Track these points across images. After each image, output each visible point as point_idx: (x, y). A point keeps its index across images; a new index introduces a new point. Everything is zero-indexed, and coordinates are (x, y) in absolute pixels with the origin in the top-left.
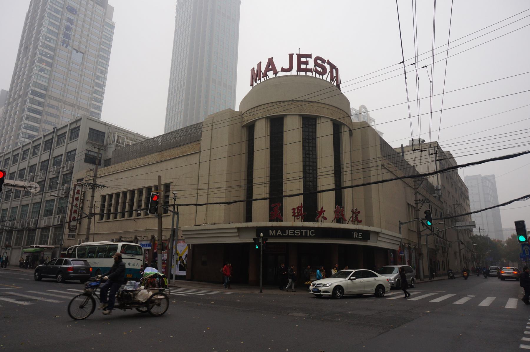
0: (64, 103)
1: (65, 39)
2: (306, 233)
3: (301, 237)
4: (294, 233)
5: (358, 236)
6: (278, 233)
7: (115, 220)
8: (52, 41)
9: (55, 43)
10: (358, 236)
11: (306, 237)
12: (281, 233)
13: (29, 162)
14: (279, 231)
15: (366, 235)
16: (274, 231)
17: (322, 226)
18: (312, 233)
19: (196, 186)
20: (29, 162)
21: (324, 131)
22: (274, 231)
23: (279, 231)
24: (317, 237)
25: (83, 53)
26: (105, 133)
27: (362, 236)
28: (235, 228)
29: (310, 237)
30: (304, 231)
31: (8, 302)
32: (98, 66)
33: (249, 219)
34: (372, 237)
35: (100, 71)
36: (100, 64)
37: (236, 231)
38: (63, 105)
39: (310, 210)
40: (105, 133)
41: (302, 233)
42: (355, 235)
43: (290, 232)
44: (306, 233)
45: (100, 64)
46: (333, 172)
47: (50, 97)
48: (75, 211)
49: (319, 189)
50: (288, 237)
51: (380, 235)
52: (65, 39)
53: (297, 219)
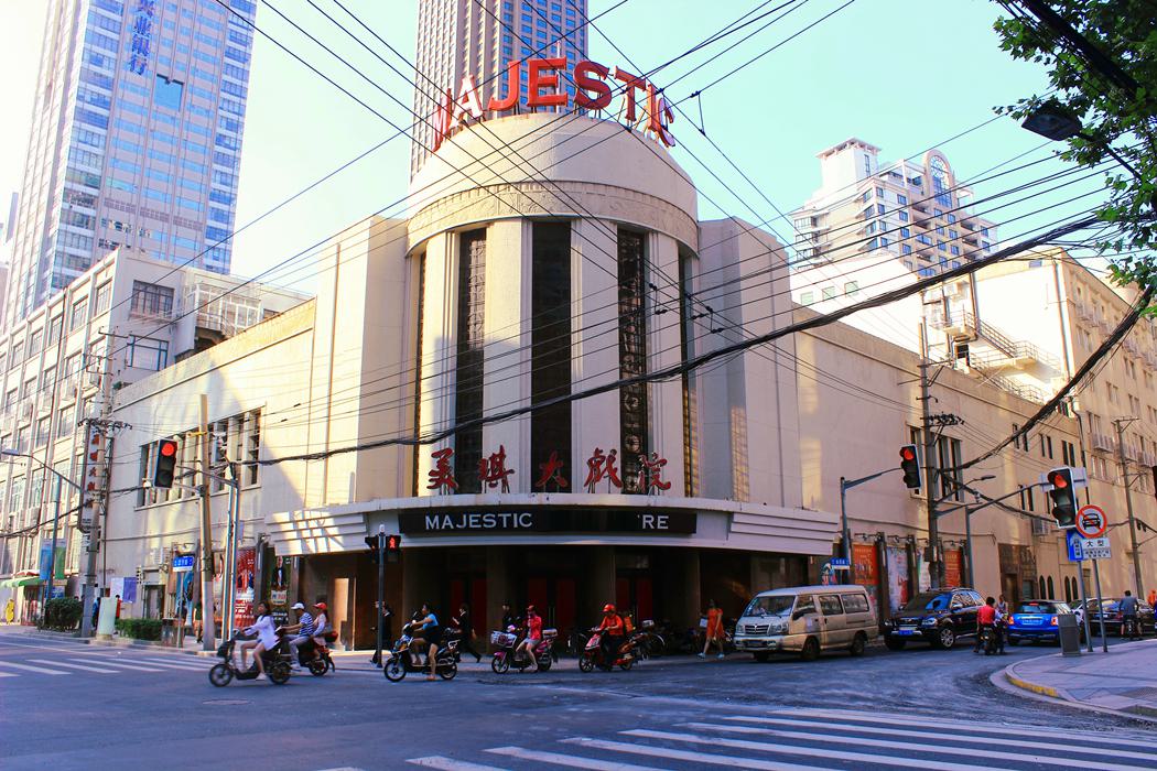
0: (142, 214)
1: (135, 52)
2: (510, 520)
3: (499, 530)
4: (481, 521)
5: (655, 523)
6: (445, 524)
7: (221, 492)
8: (106, 63)
9: (112, 66)
10: (655, 523)
11: (511, 530)
12: (450, 524)
13: (23, 374)
14: (447, 517)
15: (683, 521)
16: (437, 518)
17: (551, 502)
18: (526, 520)
19: (312, 417)
20: (23, 374)
21: (663, 256)
22: (437, 518)
23: (447, 517)
24: (537, 529)
25: (182, 84)
26: (172, 290)
27: (668, 522)
28: (359, 514)
29: (521, 531)
30: (505, 516)
31: (705, 764)
32: (221, 112)
33: (167, 499)
34: (701, 522)
35: (224, 123)
36: (225, 106)
37: (360, 519)
38: (141, 218)
39: (636, 457)
40: (172, 290)
41: (499, 520)
42: (647, 520)
43: (472, 520)
44: (510, 520)
45: (225, 106)
46: (485, 380)
47: (109, 203)
48: (91, 486)
49: (485, 415)
50: (468, 531)
51: (737, 518)
52: (135, 52)
53: (492, 486)
